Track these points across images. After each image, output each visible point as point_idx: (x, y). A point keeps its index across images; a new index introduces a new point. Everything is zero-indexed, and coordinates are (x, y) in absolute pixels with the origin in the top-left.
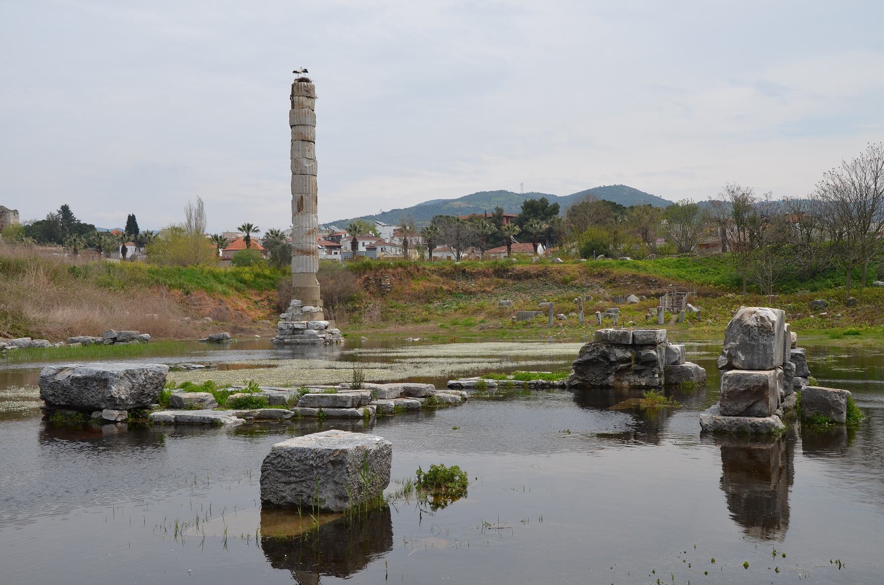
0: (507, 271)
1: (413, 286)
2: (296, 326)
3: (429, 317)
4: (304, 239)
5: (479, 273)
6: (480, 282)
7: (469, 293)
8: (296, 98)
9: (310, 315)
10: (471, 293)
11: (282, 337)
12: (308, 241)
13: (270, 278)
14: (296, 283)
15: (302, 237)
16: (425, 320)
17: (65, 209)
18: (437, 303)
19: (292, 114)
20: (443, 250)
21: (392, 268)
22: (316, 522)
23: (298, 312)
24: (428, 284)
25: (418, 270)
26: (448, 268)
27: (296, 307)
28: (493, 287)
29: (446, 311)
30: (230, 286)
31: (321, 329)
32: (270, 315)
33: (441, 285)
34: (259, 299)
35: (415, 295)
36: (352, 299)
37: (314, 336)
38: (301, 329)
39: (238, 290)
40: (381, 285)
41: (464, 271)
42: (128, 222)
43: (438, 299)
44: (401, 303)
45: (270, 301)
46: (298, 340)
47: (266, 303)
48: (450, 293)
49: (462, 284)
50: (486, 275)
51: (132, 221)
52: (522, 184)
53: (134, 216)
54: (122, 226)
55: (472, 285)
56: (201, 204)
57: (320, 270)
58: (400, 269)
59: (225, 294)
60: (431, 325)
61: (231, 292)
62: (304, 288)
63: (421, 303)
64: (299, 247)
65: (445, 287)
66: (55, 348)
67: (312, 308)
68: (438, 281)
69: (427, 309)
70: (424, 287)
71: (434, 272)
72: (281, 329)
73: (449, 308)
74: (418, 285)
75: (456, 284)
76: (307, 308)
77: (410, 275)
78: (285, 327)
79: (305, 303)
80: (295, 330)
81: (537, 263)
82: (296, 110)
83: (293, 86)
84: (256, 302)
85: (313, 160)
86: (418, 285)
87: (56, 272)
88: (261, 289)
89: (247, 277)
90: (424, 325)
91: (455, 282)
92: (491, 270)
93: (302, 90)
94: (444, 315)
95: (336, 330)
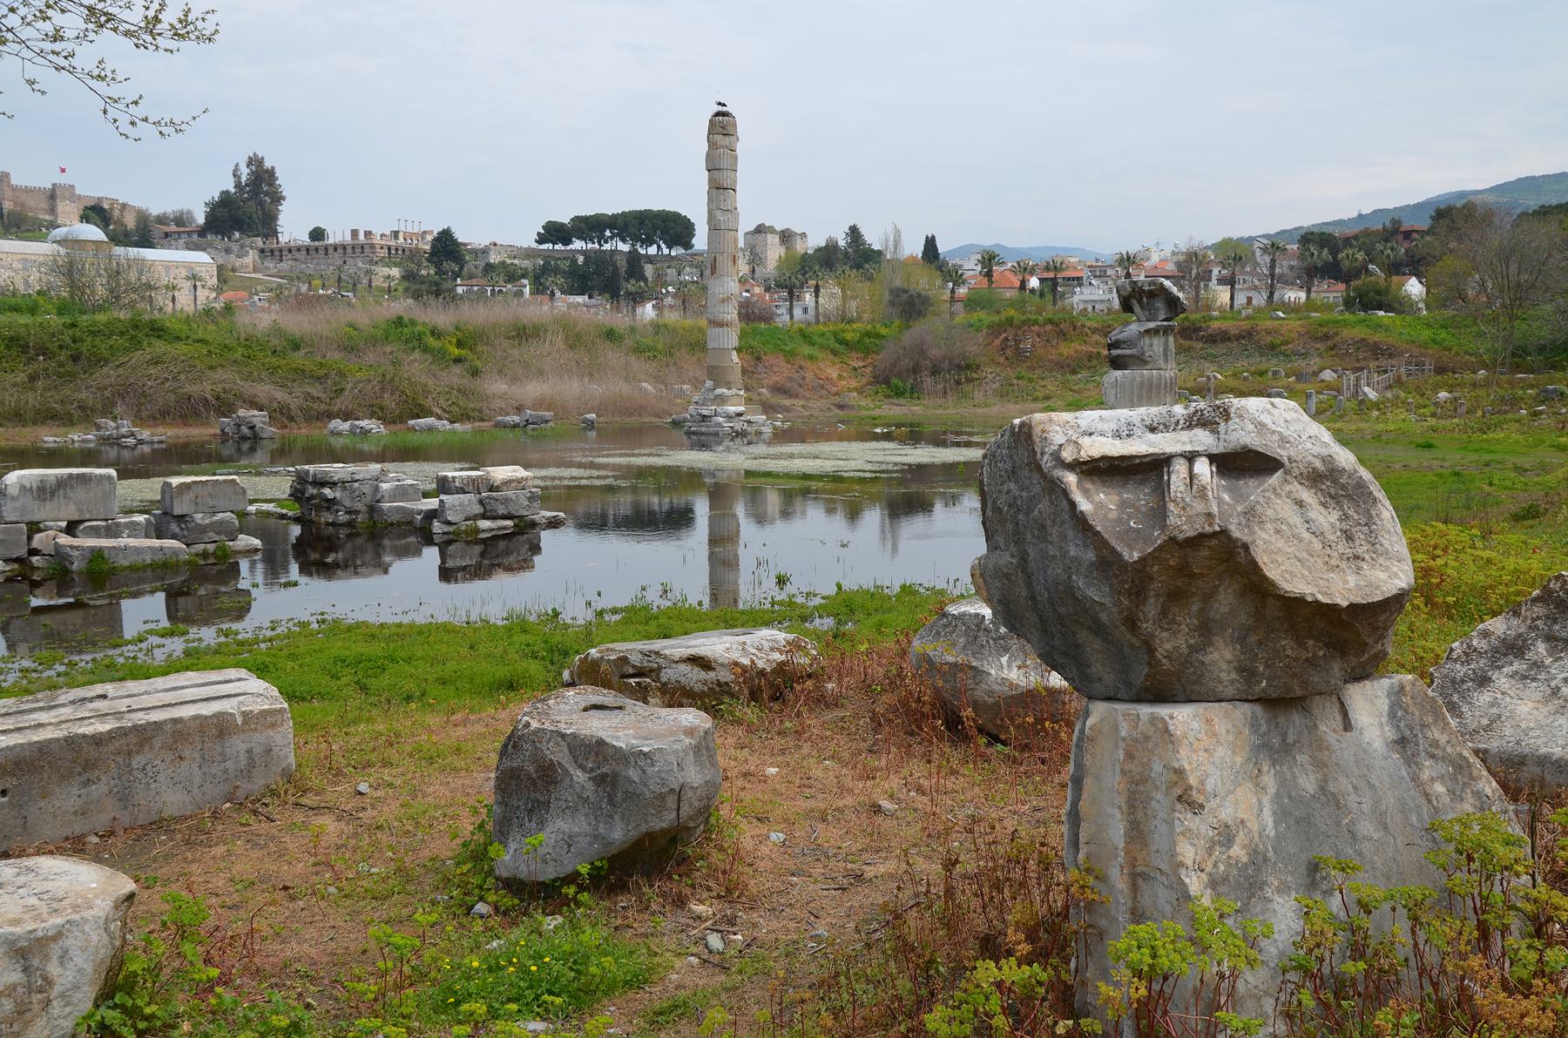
0: (1200, 329)
2: (705, 412)
17: (854, 232)
19: (710, 157)
22: (225, 626)
30: (822, 347)
35: (1057, 363)
36: (968, 367)
37: (719, 425)
39: (834, 353)
51: (930, 244)
53: (255, 162)
56: (897, 233)
58: (1049, 327)
59: (811, 358)
66: (454, 432)
74: (1067, 349)
76: (719, 391)
77: (1062, 335)
81: (1248, 318)
86: (1067, 349)
87: (578, 336)
89: (849, 336)
93: (722, 125)
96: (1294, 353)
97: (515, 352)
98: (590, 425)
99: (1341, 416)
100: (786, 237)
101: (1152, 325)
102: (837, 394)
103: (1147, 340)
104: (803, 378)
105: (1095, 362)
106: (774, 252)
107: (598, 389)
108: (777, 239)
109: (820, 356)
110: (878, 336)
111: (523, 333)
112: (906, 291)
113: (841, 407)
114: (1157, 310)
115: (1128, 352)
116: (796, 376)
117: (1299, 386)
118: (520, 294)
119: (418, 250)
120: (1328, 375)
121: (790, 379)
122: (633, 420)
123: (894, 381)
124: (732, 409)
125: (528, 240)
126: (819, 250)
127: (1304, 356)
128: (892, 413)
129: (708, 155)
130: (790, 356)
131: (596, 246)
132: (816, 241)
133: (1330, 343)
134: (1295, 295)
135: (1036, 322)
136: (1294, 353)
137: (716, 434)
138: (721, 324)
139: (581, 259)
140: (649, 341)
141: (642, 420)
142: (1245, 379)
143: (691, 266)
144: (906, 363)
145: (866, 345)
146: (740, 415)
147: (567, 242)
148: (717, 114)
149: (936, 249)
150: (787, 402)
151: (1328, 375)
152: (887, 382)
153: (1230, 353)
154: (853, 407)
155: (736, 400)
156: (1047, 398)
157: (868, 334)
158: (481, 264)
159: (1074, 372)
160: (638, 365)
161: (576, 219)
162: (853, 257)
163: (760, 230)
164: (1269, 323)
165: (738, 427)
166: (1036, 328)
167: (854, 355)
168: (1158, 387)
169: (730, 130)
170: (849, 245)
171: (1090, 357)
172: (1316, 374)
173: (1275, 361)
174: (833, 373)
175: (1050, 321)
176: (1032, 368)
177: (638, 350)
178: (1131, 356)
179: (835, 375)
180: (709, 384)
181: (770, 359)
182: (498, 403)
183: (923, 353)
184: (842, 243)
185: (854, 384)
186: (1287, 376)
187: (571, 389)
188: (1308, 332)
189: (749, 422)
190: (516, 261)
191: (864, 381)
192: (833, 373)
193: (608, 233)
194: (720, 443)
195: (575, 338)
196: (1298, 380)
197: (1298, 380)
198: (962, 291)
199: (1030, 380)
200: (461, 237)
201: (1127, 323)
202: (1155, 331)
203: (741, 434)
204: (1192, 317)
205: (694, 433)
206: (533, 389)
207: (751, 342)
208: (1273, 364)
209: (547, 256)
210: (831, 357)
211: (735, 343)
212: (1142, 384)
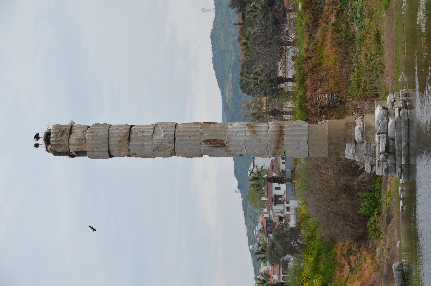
1: (331, 63)
2: (383, 148)
3: (373, 33)
4: (262, 138)
8: (73, 149)
9: (367, 130)
11: (398, 170)
12: (265, 133)
13: (319, 254)
14: (322, 152)
15: (259, 141)
16: (378, 37)
18: (355, 28)
20: (285, 67)
21: (306, 92)
23: (363, 148)
24: (328, 43)
25: (309, 58)
27: (356, 151)
29: (365, 13)
31: (387, 114)
32: (369, 251)
33: (330, 26)
34: (347, 267)
38: (387, 141)
40: (329, 107)
43: (348, 28)
44: (353, 78)
45: (350, 252)
46: (403, 144)
47: (352, 258)
48: (340, 12)
52: (203, 10)
57: (307, 120)
58: (308, 82)
60: (384, 27)
62: (329, 138)
63: (354, 49)
64: (273, 146)
65: (333, 19)
67: (357, 128)
68: (325, 31)
69: (363, 38)
70: (331, 48)
71: (311, 37)
72: (387, 170)
73: (362, 9)
75: (329, 5)
76: (357, 135)
77: (315, 69)
78: (384, 166)
79: (350, 138)
80: (389, 151)
82: (88, 148)
83: (56, 153)
84: (352, 270)
85: (155, 127)
86: (329, 56)
88: (333, 265)
90: (384, 38)
91: (326, 8)
93: (61, 142)
94: (371, 13)
95: (390, 98)
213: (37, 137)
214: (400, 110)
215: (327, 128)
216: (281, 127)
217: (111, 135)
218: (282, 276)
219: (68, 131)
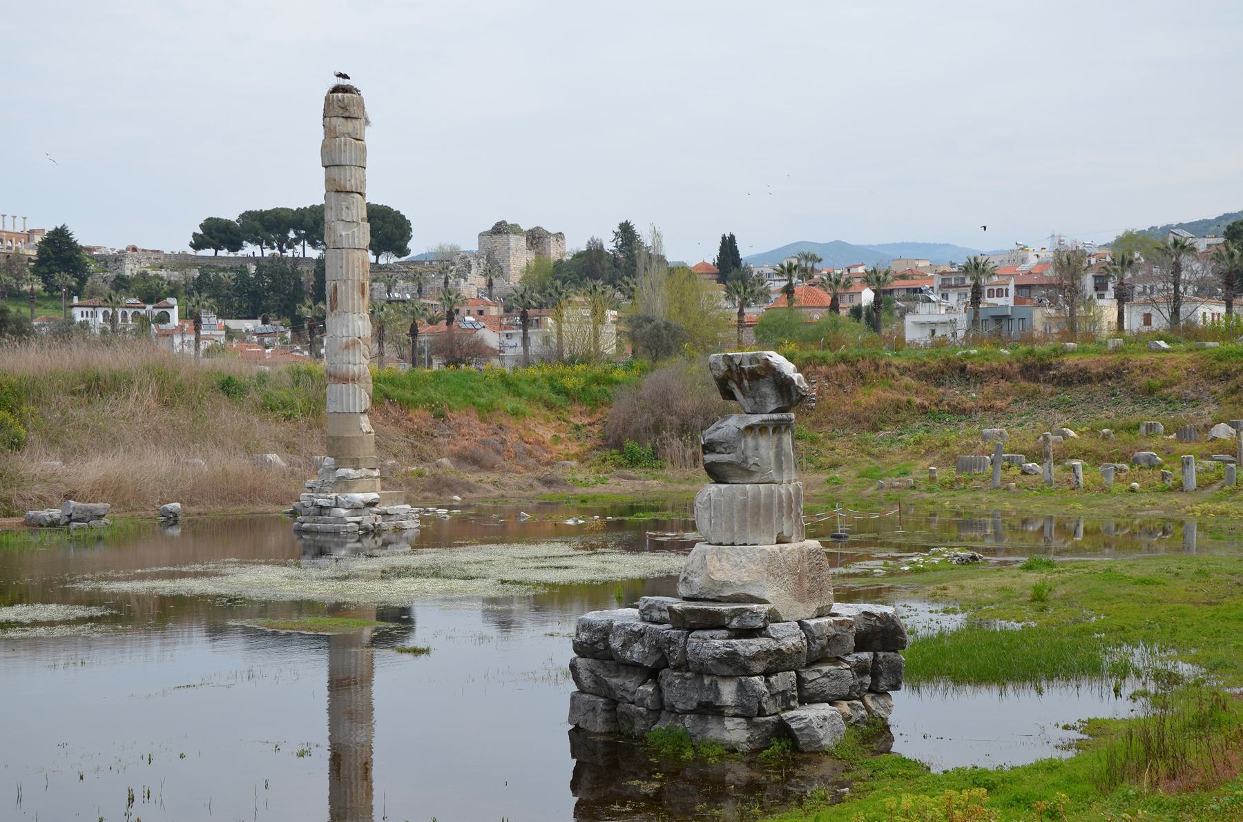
0: (1049, 367)
2: (321, 502)
5: (992, 372)
6: (989, 390)
7: (961, 412)
10: (963, 411)
17: (626, 232)
19: (326, 150)
26: (934, 363)
28: (1010, 399)
30: (531, 399)
34: (586, 420)
37: (341, 519)
38: (328, 508)
39: (549, 406)
41: (963, 369)
42: (722, 249)
49: (955, 393)
50: (1005, 376)
51: (728, 246)
53: (732, 238)
54: (710, 254)
55: (971, 396)
58: (842, 367)
59: (516, 413)
61: (528, 410)
67: (351, 471)
71: (905, 371)
74: (866, 397)
76: (342, 472)
81: (1116, 350)
84: (577, 428)
86: (866, 397)
87: (179, 390)
89: (569, 383)
92: (1016, 366)
93: (342, 103)
96: (1180, 399)
97: (81, 413)
98: (172, 519)
99: (1232, 492)
100: (536, 238)
101: (755, 419)
102: (549, 463)
103: (750, 441)
104: (503, 442)
105: (904, 414)
106: (519, 259)
107: (203, 464)
108: (523, 241)
109: (528, 410)
110: (612, 382)
111: (95, 387)
112: (649, 320)
113: (548, 482)
114: (764, 396)
115: (725, 458)
116: (492, 439)
117: (1180, 447)
118: (164, 318)
119: (19, 257)
120: (1222, 431)
121: (484, 443)
122: (239, 510)
123: (628, 444)
124: (359, 497)
125: (182, 245)
126: (579, 256)
127: (1195, 402)
128: (618, 489)
129: (324, 146)
130: (486, 411)
131: (277, 251)
132: (575, 243)
133: (1231, 384)
134: (1209, 311)
135: (823, 361)
136: (1180, 399)
137: (336, 533)
138: (344, 379)
139: (253, 269)
140: (284, 395)
141: (251, 508)
142: (1105, 437)
143: (406, 279)
144: (645, 419)
145: (592, 395)
146: (371, 504)
147: (235, 246)
148: (336, 90)
149: (735, 252)
150: (472, 478)
151: (1222, 431)
152: (619, 445)
153: (1090, 400)
154: (564, 483)
155: (367, 483)
156: (834, 466)
157: (597, 380)
158: (111, 276)
159: (875, 429)
160: (266, 429)
161: (248, 216)
162: (617, 265)
163: (500, 229)
164: (1145, 358)
165: (368, 520)
166: (824, 369)
167: (577, 408)
168: (769, 508)
169: (354, 111)
170: (620, 248)
171: (897, 408)
172: (1207, 428)
173: (1153, 411)
174: (546, 433)
175: (844, 359)
176: (817, 424)
177: (268, 407)
178: (729, 464)
179: (548, 437)
180: (329, 461)
181: (455, 416)
182: (38, 489)
183: (667, 405)
184: (609, 246)
185: (574, 448)
186: (1168, 432)
187: (152, 466)
188: (1202, 369)
189: (385, 514)
190: (163, 273)
191: (588, 445)
192: (546, 433)
193: (292, 235)
194: (341, 545)
195: (173, 391)
196: (1180, 439)
197: (1180, 439)
198: (754, 312)
199: (814, 441)
200: (82, 237)
201: (725, 414)
202: (762, 428)
203: (373, 532)
204: (1038, 349)
205: (306, 531)
206: (96, 468)
207: (432, 393)
208: (1149, 415)
209: (207, 266)
210: (544, 411)
211: (366, 403)
212: (757, 506)
213: (345, 77)
214: (358, 523)
215: (354, 435)
216: (353, 380)
217: (342, 169)
218: (995, 288)
219: (347, 114)
